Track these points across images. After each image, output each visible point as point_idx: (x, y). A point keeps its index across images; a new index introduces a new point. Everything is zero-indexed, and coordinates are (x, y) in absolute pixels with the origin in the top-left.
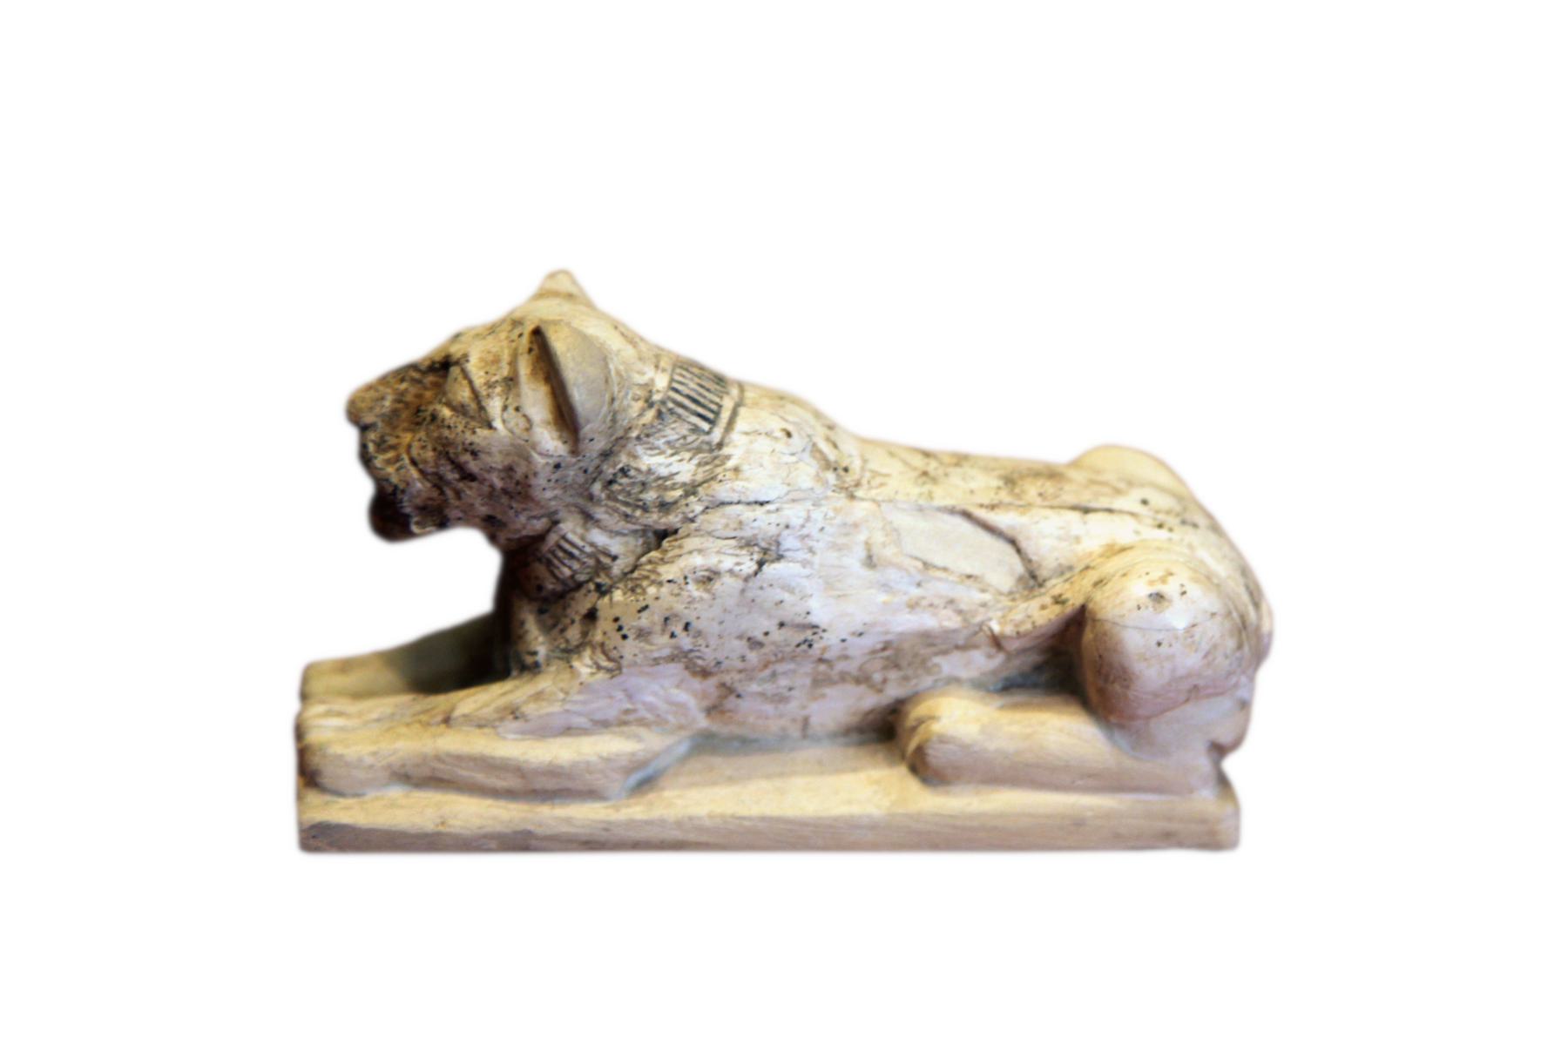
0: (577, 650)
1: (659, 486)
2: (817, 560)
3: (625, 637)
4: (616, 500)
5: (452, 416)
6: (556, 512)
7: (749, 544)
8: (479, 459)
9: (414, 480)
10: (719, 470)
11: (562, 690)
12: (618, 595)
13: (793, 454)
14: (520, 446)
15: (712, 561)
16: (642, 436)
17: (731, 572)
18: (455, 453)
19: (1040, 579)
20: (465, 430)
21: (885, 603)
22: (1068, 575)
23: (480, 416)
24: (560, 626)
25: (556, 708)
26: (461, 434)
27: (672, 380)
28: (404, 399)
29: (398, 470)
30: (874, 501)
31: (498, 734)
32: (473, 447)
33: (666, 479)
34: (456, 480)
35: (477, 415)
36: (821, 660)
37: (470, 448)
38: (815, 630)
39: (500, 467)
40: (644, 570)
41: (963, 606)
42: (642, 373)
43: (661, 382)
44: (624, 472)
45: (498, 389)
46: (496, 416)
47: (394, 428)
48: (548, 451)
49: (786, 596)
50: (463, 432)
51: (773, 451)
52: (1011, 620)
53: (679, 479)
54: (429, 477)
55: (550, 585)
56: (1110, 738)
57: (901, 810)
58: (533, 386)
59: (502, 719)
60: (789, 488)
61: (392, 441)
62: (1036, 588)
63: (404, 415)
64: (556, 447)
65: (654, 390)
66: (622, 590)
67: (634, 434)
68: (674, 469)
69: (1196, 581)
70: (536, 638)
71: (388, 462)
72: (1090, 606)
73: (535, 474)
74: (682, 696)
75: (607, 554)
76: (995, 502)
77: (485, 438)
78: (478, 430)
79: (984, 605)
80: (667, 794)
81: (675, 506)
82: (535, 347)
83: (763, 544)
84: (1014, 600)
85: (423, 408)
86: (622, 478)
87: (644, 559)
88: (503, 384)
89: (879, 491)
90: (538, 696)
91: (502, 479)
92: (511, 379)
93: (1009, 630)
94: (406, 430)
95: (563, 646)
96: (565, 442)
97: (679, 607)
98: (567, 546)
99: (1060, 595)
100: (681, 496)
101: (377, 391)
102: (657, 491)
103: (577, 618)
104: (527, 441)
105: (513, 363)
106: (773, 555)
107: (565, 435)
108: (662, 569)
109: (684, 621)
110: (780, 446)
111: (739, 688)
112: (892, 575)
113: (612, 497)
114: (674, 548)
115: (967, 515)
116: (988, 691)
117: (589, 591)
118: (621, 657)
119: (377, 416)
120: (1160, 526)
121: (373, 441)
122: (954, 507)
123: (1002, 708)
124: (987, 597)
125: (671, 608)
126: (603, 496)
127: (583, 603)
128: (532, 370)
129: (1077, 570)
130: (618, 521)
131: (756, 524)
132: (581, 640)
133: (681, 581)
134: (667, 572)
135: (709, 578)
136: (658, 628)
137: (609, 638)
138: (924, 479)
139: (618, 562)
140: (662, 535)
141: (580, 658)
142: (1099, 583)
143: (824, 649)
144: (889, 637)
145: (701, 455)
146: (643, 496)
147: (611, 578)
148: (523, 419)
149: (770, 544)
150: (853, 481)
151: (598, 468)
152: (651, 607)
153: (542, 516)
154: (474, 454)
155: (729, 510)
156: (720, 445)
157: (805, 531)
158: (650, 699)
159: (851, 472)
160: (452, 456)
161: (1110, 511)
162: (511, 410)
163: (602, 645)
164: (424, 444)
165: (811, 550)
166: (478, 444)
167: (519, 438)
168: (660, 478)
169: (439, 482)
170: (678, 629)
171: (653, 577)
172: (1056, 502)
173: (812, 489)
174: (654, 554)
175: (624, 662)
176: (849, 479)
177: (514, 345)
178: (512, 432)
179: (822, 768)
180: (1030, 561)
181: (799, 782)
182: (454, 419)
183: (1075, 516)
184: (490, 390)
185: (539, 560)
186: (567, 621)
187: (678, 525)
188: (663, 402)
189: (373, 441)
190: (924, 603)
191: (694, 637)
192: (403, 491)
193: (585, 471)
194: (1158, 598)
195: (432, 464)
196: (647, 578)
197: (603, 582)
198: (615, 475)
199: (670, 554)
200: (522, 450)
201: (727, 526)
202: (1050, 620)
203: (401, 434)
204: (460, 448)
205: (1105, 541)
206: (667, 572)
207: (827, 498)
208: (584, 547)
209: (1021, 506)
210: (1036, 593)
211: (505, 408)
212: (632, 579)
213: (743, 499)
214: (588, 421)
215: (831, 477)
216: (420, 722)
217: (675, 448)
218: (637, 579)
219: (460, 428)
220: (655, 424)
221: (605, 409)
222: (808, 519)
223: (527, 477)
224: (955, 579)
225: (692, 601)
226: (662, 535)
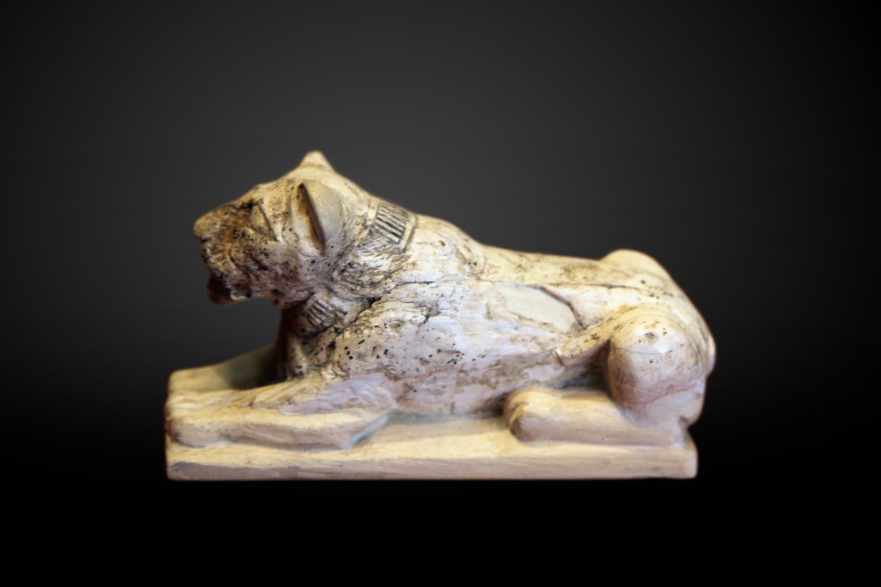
0: (324, 365)
1: (370, 273)
2: (459, 314)
3: (351, 358)
4: (346, 281)
5: (254, 234)
6: (312, 288)
7: (421, 305)
8: (269, 258)
9: (232, 269)
10: (404, 264)
11: (316, 388)
12: (347, 334)
13: (445, 255)
14: (292, 250)
15: (400, 315)
16: (361, 245)
17: (411, 321)
18: (256, 255)
19: (584, 325)
20: (261, 241)
21: (497, 339)
22: (600, 323)
23: (270, 234)
24: (315, 352)
25: (312, 398)
26: (259, 244)
27: (378, 213)
28: (227, 224)
29: (223, 264)
30: (491, 281)
31: (280, 412)
32: (266, 251)
33: (374, 269)
34: (256, 270)
35: (268, 233)
36: (461, 371)
37: (264, 252)
38: (458, 354)
39: (281, 262)
40: (362, 320)
41: (541, 341)
42: (360, 210)
43: (372, 214)
44: (351, 265)
45: (280, 219)
46: (279, 234)
47: (222, 240)
48: (308, 253)
49: (442, 335)
50: (260, 242)
51: (434, 253)
52: (568, 349)
53: (381, 269)
54: (241, 268)
55: (309, 329)
56: (624, 414)
57: (506, 455)
58: (299, 217)
59: (282, 404)
60: (443, 274)
61: (220, 248)
62: (582, 330)
63: (227, 233)
64: (312, 251)
65: (368, 219)
66: (350, 331)
67: (356, 244)
68: (378, 264)
69: (672, 326)
70: (301, 359)
71: (218, 260)
72: (613, 340)
73: (301, 266)
74: (383, 391)
75: (341, 311)
76: (559, 282)
77: (273, 246)
78: (269, 242)
79: (553, 340)
80: (375, 446)
81: (379, 284)
82: (301, 195)
83: (429, 306)
84: (570, 337)
85: (238, 229)
86: (349, 268)
87: (362, 314)
88: (283, 216)
89: (494, 276)
90: (302, 391)
91: (282, 269)
92: (287, 213)
93: (567, 354)
94: (228, 242)
95: (316, 363)
96: (318, 248)
97: (382, 341)
98: (319, 307)
99: (596, 334)
100: (383, 279)
101: (212, 219)
102: (369, 276)
103: (324, 347)
104: (296, 248)
105: (288, 204)
106: (434, 312)
107: (317, 244)
108: (372, 320)
109: (385, 349)
110: (438, 251)
111: (415, 386)
112: (501, 323)
113: (344, 279)
114: (379, 308)
115: (543, 289)
116: (555, 388)
117: (331, 332)
118: (349, 369)
119: (212, 234)
120: (652, 296)
121: (210, 248)
122: (536, 285)
123: (563, 397)
124: (554, 335)
125: (377, 342)
126: (339, 278)
127: (327, 339)
128: (299, 208)
129: (605, 320)
130: (348, 293)
131: (425, 294)
132: (327, 360)
133: (383, 326)
134: (375, 321)
135: (398, 325)
136: (370, 353)
137: (342, 358)
138: (519, 269)
139: (347, 316)
140: (372, 300)
141: (326, 369)
142: (617, 328)
143: (463, 365)
144: (499, 358)
145: (394, 256)
146: (361, 279)
147: (343, 325)
148: (294, 236)
149: (433, 306)
150: (479, 270)
151: (336, 263)
152: (366, 341)
153: (305, 290)
154: (267, 255)
155: (410, 286)
156: (405, 250)
157: (452, 298)
158: (365, 392)
159: (478, 265)
160: (254, 256)
161: (624, 287)
162: (287, 230)
163: (338, 362)
164: (238, 249)
165: (456, 309)
166: (269, 250)
167: (292, 246)
168: (371, 269)
169: (246, 271)
170: (381, 353)
171: (367, 324)
172: (593, 282)
173: (456, 275)
174: (367, 311)
175: (351, 372)
176: (477, 269)
177: (289, 194)
178: (287, 242)
179: (462, 431)
180: (579, 315)
181: (449, 439)
182: (255, 235)
183: (604, 290)
184: (275, 219)
185: (303, 315)
186: (319, 349)
187: (381, 295)
188: (373, 226)
189: (210, 248)
190: (519, 339)
191: (390, 358)
192: (226, 276)
193: (329, 265)
194: (651, 336)
195: (243, 261)
196: (363, 324)
197: (339, 327)
198: (345, 267)
199: (377, 311)
200: (293, 253)
201: (408, 295)
202: (590, 348)
203: (225, 244)
204: (258, 252)
205: (621, 304)
206: (375, 321)
207: (464, 280)
208: (328, 307)
209: (574, 284)
210: (582, 333)
211: (284, 229)
212: (355, 325)
213: (418, 280)
214: (330, 237)
215: (467, 268)
216: (236, 405)
217: (379, 252)
218: (358, 325)
219: (259, 240)
220: (368, 238)
221: (340, 230)
222: (454, 292)
223: (296, 268)
224: (537, 325)
225: (389, 338)
226: (372, 300)
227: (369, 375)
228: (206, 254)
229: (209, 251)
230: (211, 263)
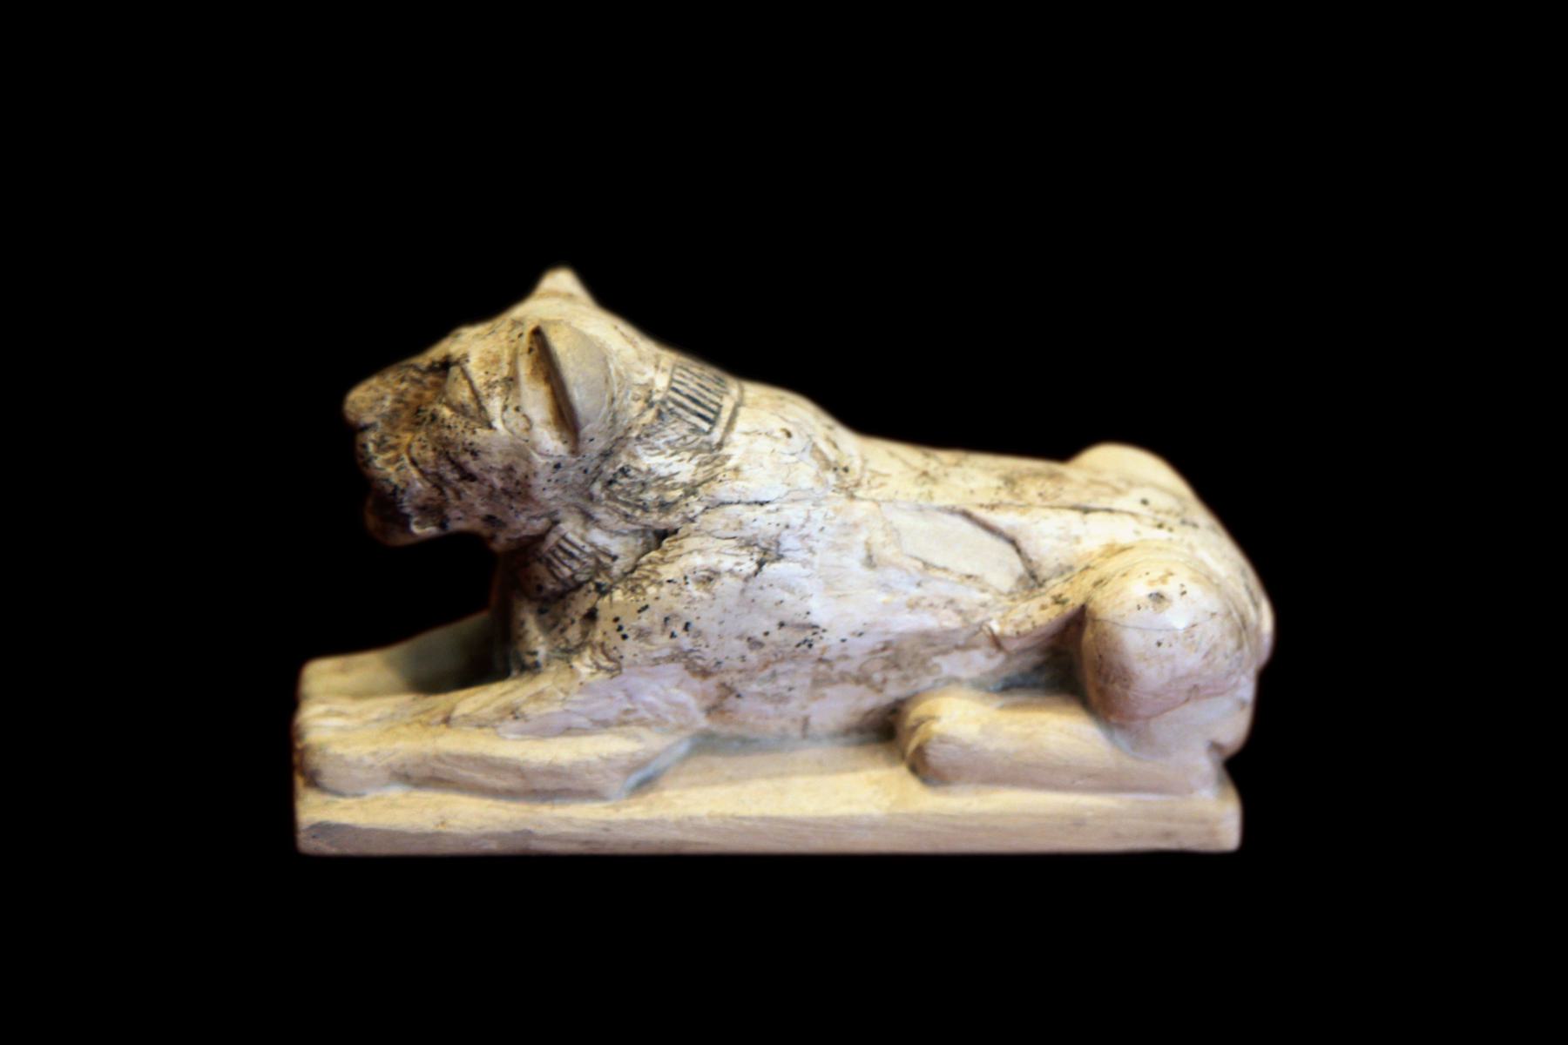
0: (577, 650)
1: (659, 486)
2: (817, 560)
3: (625, 637)
4: (616, 500)
5: (452, 416)
6: (556, 512)
7: (749, 544)
8: (479, 459)
9: (414, 480)
10: (719, 470)
11: (562, 690)
12: (618, 595)
13: (793, 454)
14: (520, 446)
15: (712, 561)
16: (642, 436)
17: (731, 572)
18: (455, 453)
19: (1040, 579)
20: (465, 430)
21: (885, 603)
22: (1068, 575)
23: (480, 416)
24: (560, 626)
25: (556, 708)
26: (461, 434)
27: (672, 380)
28: (404, 399)
29: (398, 470)
30: (874, 501)
31: (498, 734)
32: (473, 447)
33: (666, 479)
34: (456, 480)
35: (477, 415)
36: (821, 660)
37: (470, 448)
38: (815, 630)
39: (500, 467)
40: (644, 570)
41: (963, 606)
42: (642, 373)
43: (661, 382)
44: (624, 472)
45: (498, 389)
46: (496, 416)
47: (394, 428)
48: (548, 451)
49: (786, 596)
50: (463, 432)
51: (773, 451)
52: (1011, 620)
53: (679, 479)
54: (429, 477)
55: (550, 585)
56: (1110, 738)
57: (901, 810)
58: (533, 386)
59: (502, 719)
60: (789, 488)
61: (392, 441)
62: (1036, 588)
63: (404, 415)
64: (556, 447)
65: (654, 390)
66: (622, 590)
67: (634, 434)
68: (674, 469)
69: (1196, 581)
70: (536, 638)
71: (388, 462)
72: (1090, 606)
73: (535, 474)
74: (682, 696)
75: (607, 554)
76: (995, 502)
77: (485, 438)
78: (478, 430)
79: (984, 605)
80: (667, 794)
81: (675, 506)
82: (535, 347)
83: (763, 544)
84: (1014, 600)
85: (423, 408)
86: (622, 478)
87: (644, 559)
88: (503, 384)
89: (879, 491)
90: (538, 696)
91: (502, 479)
92: (511, 379)
93: (1009, 630)
94: (406, 430)
95: (563, 646)
96: (565, 442)
97: (679, 607)
98: (567, 546)
99: (1060, 595)
100: (681, 496)
101: (377, 390)
102: (657, 491)
103: (577, 618)
104: (527, 441)
105: (513, 363)
106: (773, 555)
107: (565, 435)
108: (662, 569)
109: (684, 621)
110: (780, 446)
111: (739, 688)
112: (892, 575)
113: (612, 497)
114: (674, 548)
115: (967, 515)
116: (988, 691)
117: (589, 591)
118: (621, 657)
119: (377, 416)
120: (1160, 526)
121: (373, 441)
122: (954, 507)
123: (1002, 708)
124: (987, 597)
125: (671, 608)
126: (603, 496)
127: (583, 603)
128: (532, 370)
129: (1077, 570)
130: (618, 521)
131: (756, 524)
132: (581, 640)
133: (681, 581)
134: (667, 572)
135: (709, 578)
136: (658, 628)
137: (609, 638)
138: (924, 479)
139: (618, 562)
140: (662, 535)
141: (580, 658)
142: (1099, 583)
143: (824, 649)
144: (889, 637)
145: (701, 455)
146: (643, 496)
147: (611, 578)
148: (523, 419)
149: (770, 544)
150: (853, 481)
151: (598, 468)
152: (651, 607)
153: (542, 516)
154: (474, 454)
155: (729, 510)
156: (720, 445)
157: (805, 531)
158: (650, 699)
159: (851, 472)
160: (452, 456)
161: (1110, 511)
162: (511, 410)
163: (602, 645)
164: (424, 444)
165: (811, 550)
166: (478, 444)
167: (519, 438)
168: (660, 478)
169: (439, 482)
170: (678, 629)
171: (653, 577)
172: (1056, 502)
173: (812, 489)
174: (654, 554)
175: (624, 662)
176: (849, 479)
177: (514, 345)
178: (512, 432)
179: (822, 768)
180: (1030, 561)
181: (799, 782)
182: (454, 419)
183: (1075, 516)
184: (490, 390)
185: (539, 560)
186: (567, 621)
187: (678, 525)
188: (663, 402)
189: (373, 441)
190: (924, 603)
191: (694, 637)
192: (403, 491)
193: (585, 471)
194: (1158, 598)
195: (432, 464)
196: (647, 578)
197: (603, 582)
198: (615, 475)
199: (670, 554)
200: (522, 450)
201: (727, 526)
202: (1050, 620)
203: (401, 434)
204: (460, 448)
205: (1105, 541)
206: (667, 572)
207: (827, 498)
208: (584, 547)
209: (1021, 506)
210: (1036, 593)
211: (505, 408)
212: (632, 579)
213: (743, 499)
214: (588, 421)
215: (831, 477)
216: (420, 722)
217: (675, 448)
218: (637, 579)
219: (460, 428)
220: (655, 424)
221: (605, 409)
222: (808, 519)
223: (527, 477)
224: (955, 579)
225: (692, 601)
226: (662, 535)
227: (657, 668)
228: (367, 453)
229: (371, 447)
230: (376, 468)
